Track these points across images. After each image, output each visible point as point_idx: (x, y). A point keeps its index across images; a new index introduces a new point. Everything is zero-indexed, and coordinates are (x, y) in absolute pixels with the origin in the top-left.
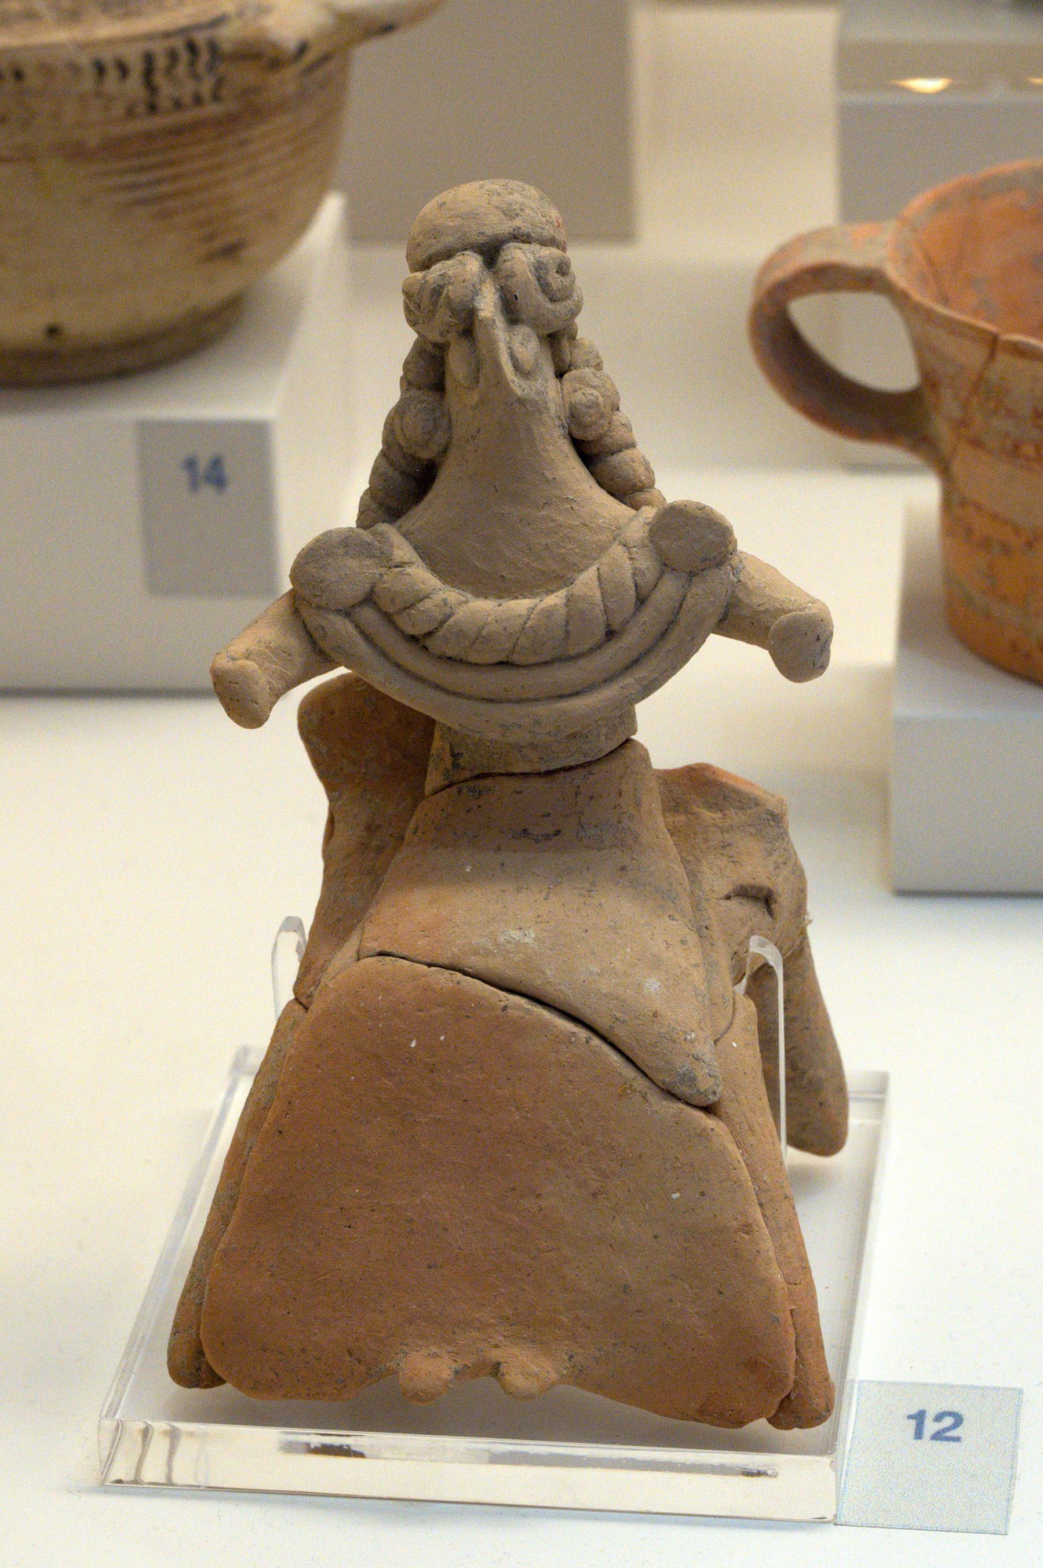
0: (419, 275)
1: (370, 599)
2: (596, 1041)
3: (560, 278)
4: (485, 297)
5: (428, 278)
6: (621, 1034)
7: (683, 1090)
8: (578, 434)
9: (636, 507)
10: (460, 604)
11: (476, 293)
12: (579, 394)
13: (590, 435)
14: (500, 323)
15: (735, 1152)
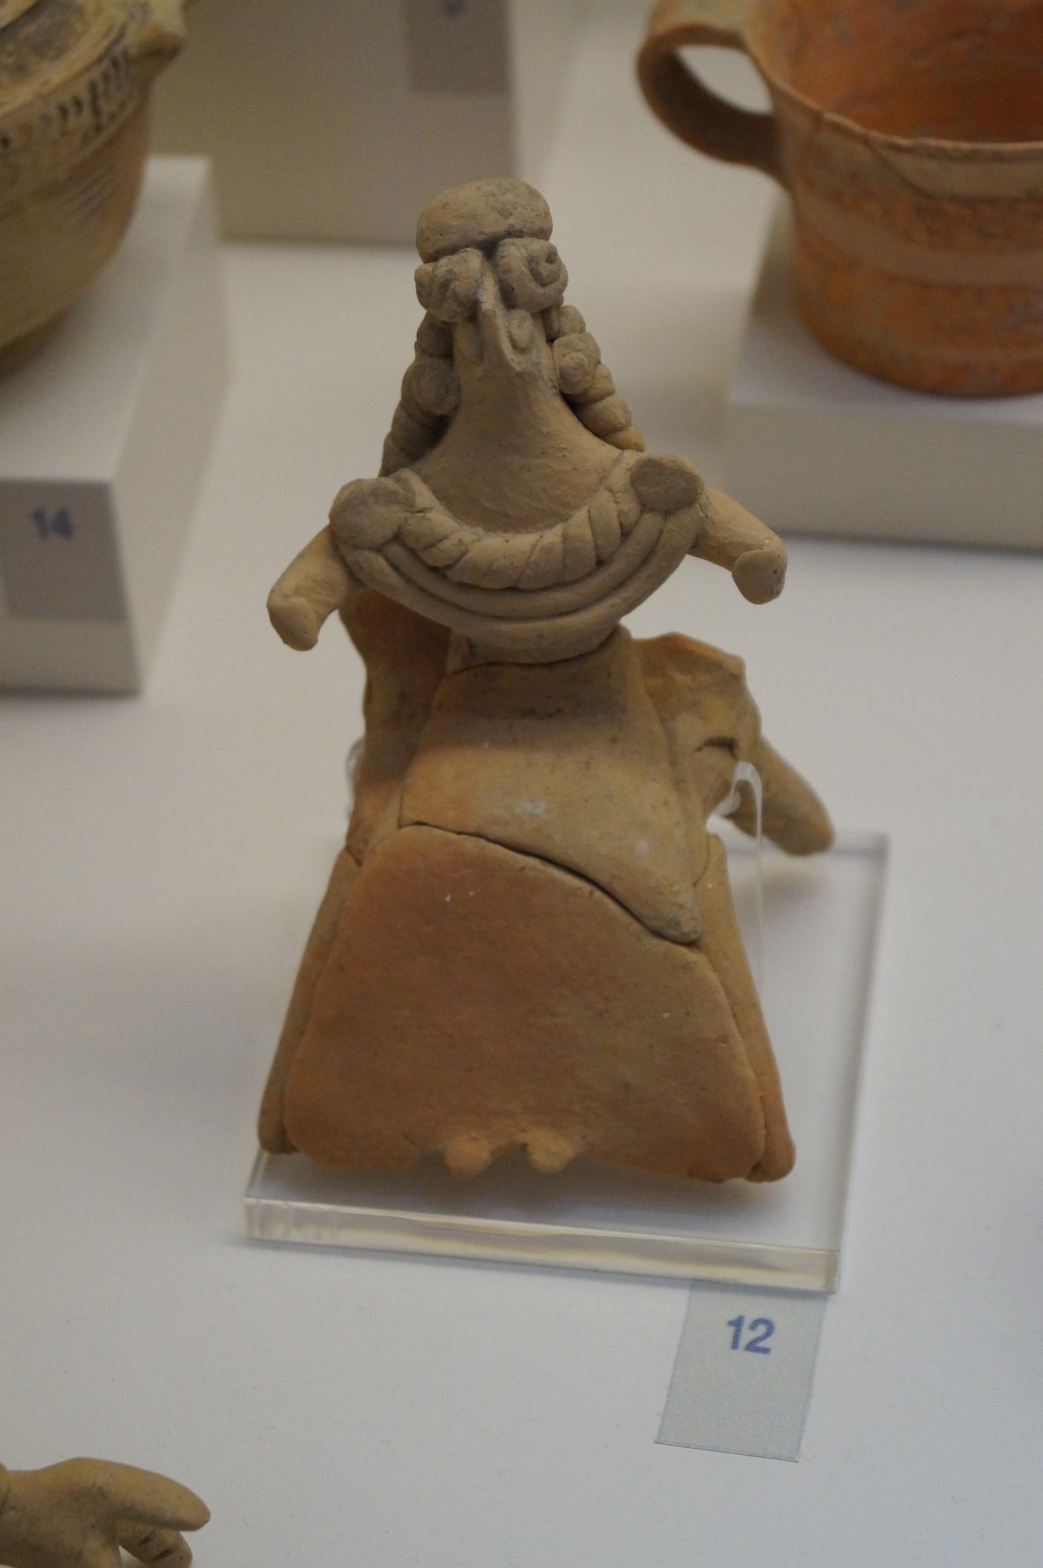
0: (429, 267)
1: (397, 537)
2: (598, 894)
3: (549, 266)
4: (486, 290)
5: (438, 272)
6: (617, 887)
7: (672, 932)
8: (567, 391)
9: (621, 446)
10: (474, 541)
11: (478, 285)
12: (567, 358)
13: (578, 390)
14: (500, 310)
15: (712, 976)
